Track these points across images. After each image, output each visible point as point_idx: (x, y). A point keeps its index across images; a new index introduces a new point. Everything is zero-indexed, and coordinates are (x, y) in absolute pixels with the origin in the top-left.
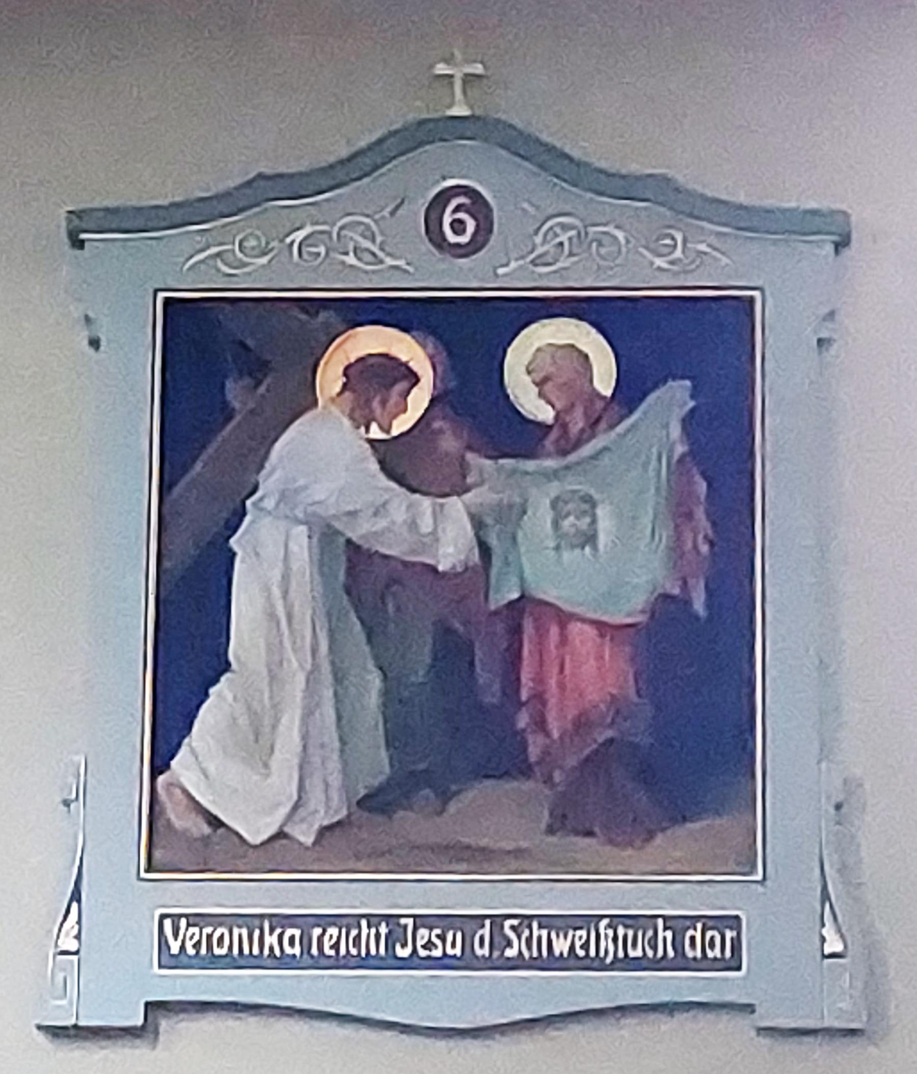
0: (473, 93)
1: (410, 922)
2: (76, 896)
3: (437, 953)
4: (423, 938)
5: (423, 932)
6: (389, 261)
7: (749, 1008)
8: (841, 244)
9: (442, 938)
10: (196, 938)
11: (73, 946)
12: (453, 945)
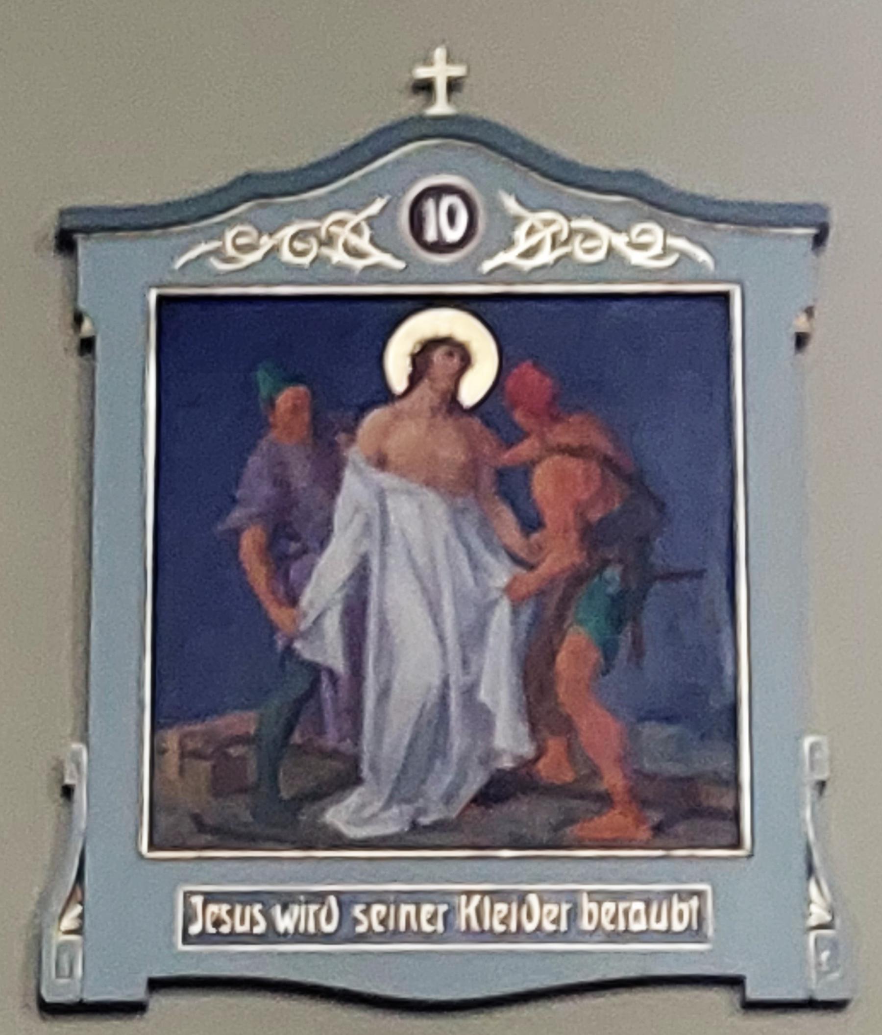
0: (456, 95)
1: (198, 901)
2: (810, 870)
3: (225, 929)
4: (378, 913)
5: (213, 908)
6: (377, 257)
7: (735, 982)
8: (819, 240)
9: (231, 913)
10: (502, 915)
11: (586, 925)
12: (242, 922)
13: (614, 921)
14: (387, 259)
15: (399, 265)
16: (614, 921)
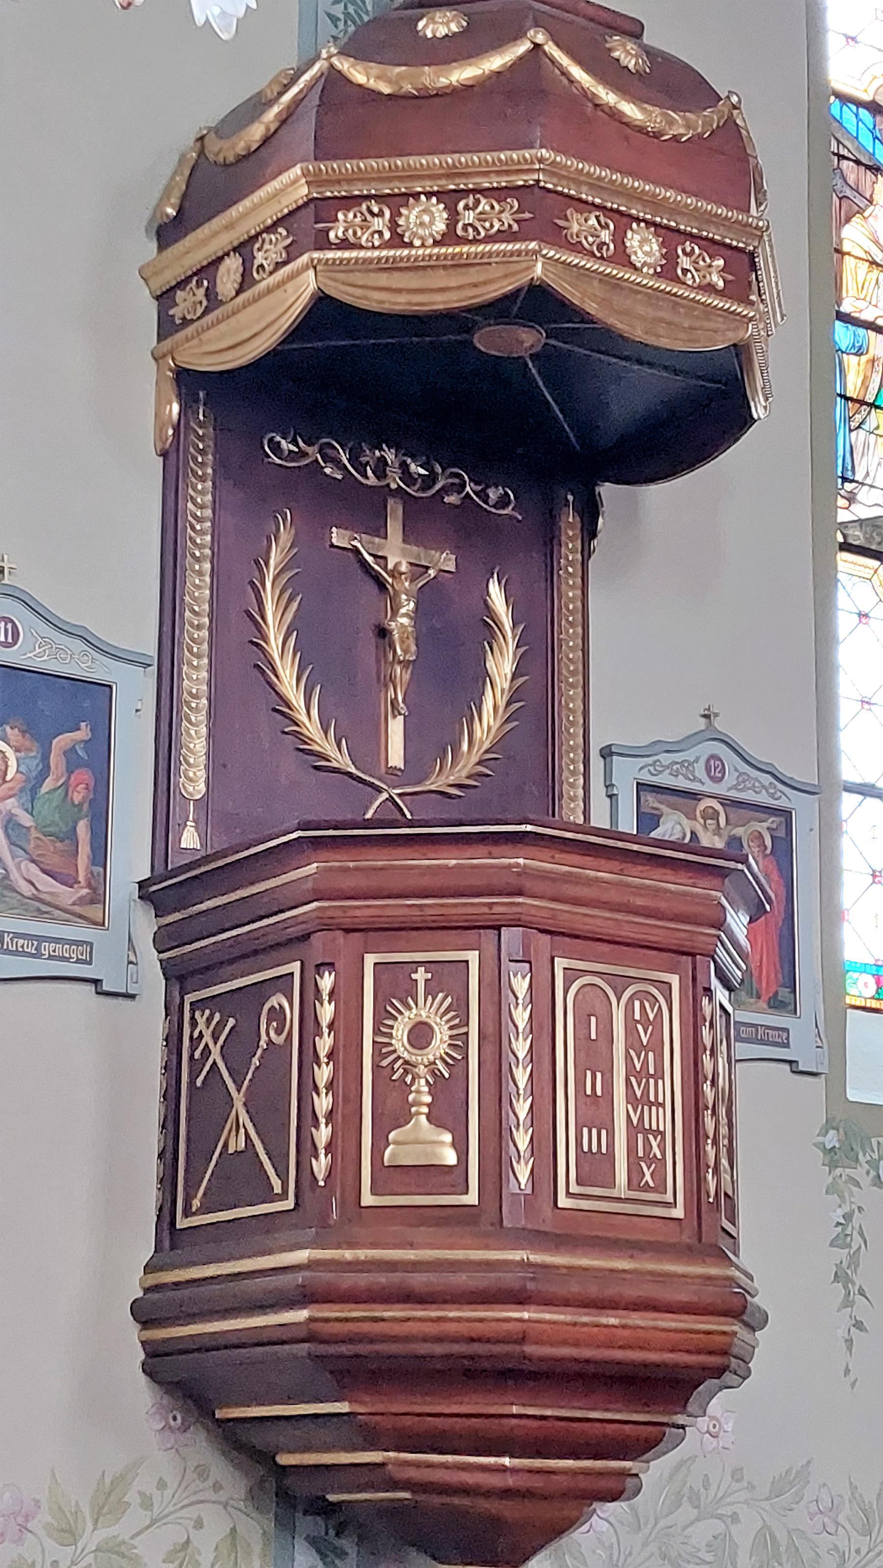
7: (96, 982)
13: (54, 951)
16: (54, 951)
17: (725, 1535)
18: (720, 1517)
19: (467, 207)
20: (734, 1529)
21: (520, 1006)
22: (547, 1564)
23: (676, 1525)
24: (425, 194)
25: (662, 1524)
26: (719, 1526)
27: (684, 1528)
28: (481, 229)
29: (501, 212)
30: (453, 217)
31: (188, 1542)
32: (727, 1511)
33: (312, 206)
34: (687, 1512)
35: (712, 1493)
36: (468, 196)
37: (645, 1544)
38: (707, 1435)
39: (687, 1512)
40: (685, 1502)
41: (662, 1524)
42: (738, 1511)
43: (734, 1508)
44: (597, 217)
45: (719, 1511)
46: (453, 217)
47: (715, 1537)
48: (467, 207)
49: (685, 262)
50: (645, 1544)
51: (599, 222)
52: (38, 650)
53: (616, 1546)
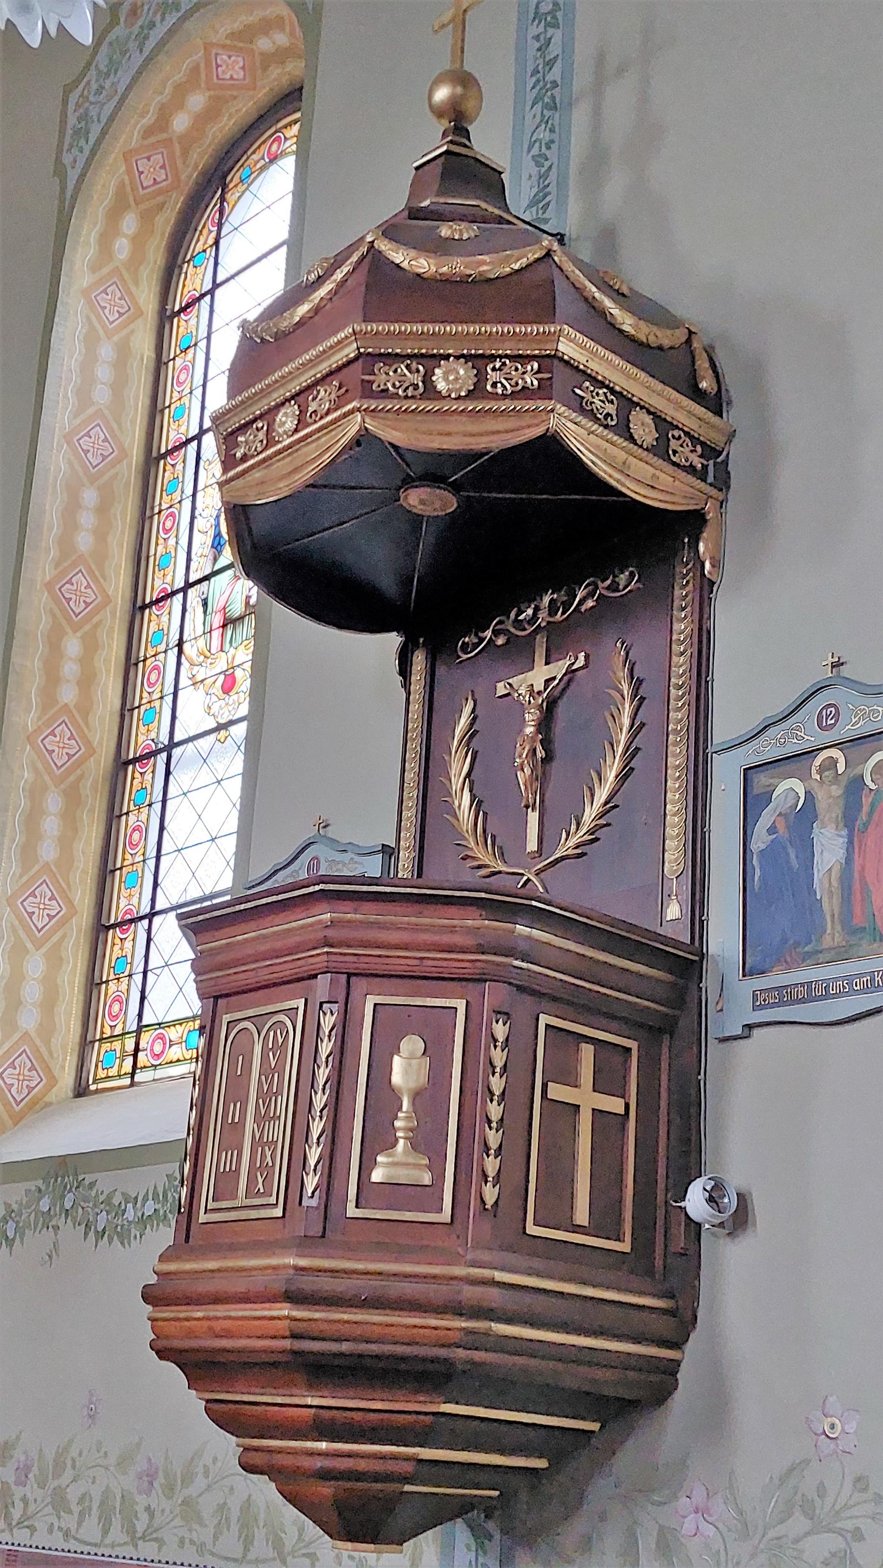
14: (809, 738)
15: (813, 739)
17: (846, 1552)
18: (840, 1532)
19: (494, 369)
20: (854, 1545)
21: (497, 1075)
22: (447, 1550)
23: (786, 1536)
24: (455, 357)
25: (771, 1534)
26: (835, 1543)
27: (797, 1541)
28: (508, 387)
29: (524, 373)
30: (481, 377)
31: (225, 1503)
32: (849, 1525)
33: (360, 361)
34: (798, 1523)
35: (829, 1501)
36: (495, 361)
37: (753, 1556)
38: (824, 1436)
39: (798, 1523)
40: (798, 1513)
41: (771, 1534)
42: (861, 1526)
43: (858, 1523)
44: (605, 394)
45: (839, 1525)
46: (481, 377)
47: (834, 1555)
48: (494, 369)
49: (674, 444)
50: (753, 1556)
51: (606, 397)
52: (854, 721)
53: (722, 1553)
